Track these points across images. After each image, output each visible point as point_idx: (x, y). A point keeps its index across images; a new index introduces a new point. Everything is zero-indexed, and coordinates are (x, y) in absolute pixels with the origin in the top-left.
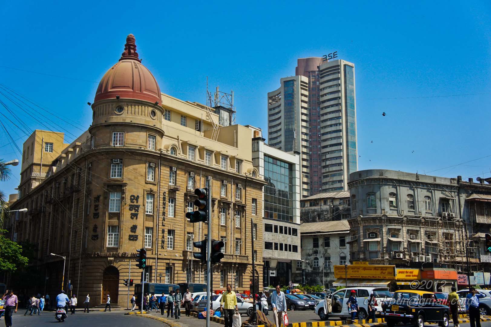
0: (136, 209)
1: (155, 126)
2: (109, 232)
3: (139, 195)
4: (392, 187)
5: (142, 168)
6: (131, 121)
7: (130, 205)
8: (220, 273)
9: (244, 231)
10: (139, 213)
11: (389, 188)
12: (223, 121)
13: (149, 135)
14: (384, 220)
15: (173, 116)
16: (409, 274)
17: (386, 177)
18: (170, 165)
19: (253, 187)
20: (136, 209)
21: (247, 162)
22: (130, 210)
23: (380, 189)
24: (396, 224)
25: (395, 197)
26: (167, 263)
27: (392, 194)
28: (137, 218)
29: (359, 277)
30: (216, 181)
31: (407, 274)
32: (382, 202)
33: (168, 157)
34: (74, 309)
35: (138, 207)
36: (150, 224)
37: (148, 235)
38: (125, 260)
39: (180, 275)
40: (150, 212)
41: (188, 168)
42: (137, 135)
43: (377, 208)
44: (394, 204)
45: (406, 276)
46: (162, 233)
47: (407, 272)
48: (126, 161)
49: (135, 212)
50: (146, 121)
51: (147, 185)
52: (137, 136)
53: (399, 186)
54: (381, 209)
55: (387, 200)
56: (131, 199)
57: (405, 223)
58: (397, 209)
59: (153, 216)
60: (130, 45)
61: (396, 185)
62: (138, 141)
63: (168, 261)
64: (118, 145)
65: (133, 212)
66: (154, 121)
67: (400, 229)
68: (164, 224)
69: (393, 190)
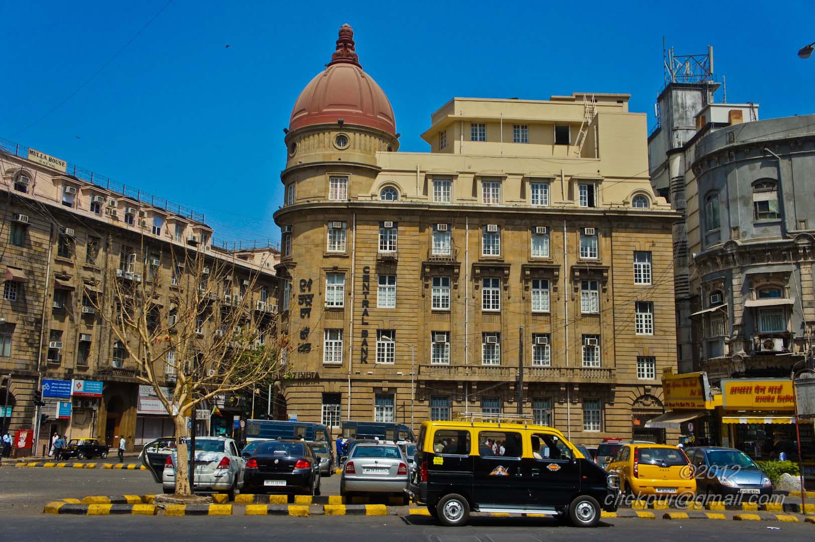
1: (341, 161)
2: (326, 339)
3: (312, 279)
4: (762, 167)
5: (321, 234)
7: (299, 296)
10: (312, 307)
11: (751, 169)
12: (681, 110)
15: (489, 131)
16: (767, 394)
17: (743, 142)
19: (636, 228)
23: (726, 176)
27: (759, 185)
28: (309, 316)
29: (694, 405)
30: (516, 233)
31: (761, 394)
33: (365, 207)
34: (119, 454)
35: (311, 297)
36: (336, 324)
37: (334, 342)
38: (293, 385)
42: (311, 182)
43: (720, 228)
44: (773, 208)
45: (758, 399)
47: (758, 389)
49: (307, 306)
50: (324, 156)
51: (327, 259)
52: (310, 184)
53: (790, 157)
54: (730, 227)
55: (746, 200)
56: (301, 286)
57: (805, 256)
58: (780, 220)
59: (500, 313)
60: (345, 41)
61: (774, 157)
62: (312, 192)
63: (376, 384)
65: (304, 306)
66: (340, 152)
67: (788, 274)
68: (365, 321)
69: (769, 173)
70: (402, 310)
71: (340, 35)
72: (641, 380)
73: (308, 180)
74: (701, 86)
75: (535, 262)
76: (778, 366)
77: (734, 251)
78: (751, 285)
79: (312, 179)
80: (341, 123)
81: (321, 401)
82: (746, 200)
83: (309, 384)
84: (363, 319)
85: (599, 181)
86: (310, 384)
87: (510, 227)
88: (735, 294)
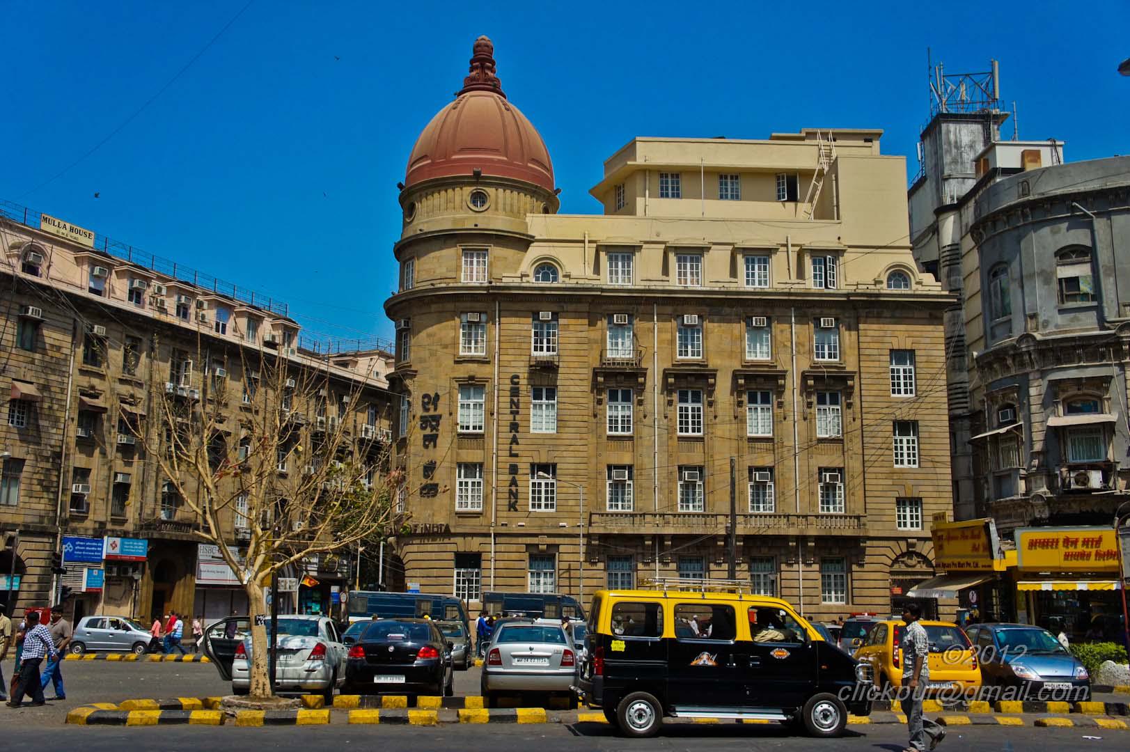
0: (434, 423)
5: (451, 330)
6: (476, 225)
7: (421, 417)
8: (816, 567)
9: (856, 446)
11: (1054, 233)
12: (954, 151)
13: (463, 250)
14: (1029, 353)
15: (684, 184)
16: (1080, 548)
17: (1043, 194)
18: (534, 309)
20: (434, 423)
21: (879, 250)
22: (423, 428)
23: (1019, 243)
24: (1088, 361)
25: (1087, 259)
26: (528, 546)
27: (1066, 254)
28: (435, 446)
29: (977, 566)
30: (724, 326)
31: (1071, 549)
32: (1026, 289)
35: (437, 419)
37: (470, 481)
39: (577, 574)
40: (474, 428)
41: (604, 307)
44: (1085, 287)
45: (1067, 556)
46: (510, 474)
47: (1067, 542)
48: (416, 320)
49: (432, 431)
50: (455, 221)
52: (435, 260)
54: (1025, 315)
55: (1047, 277)
56: (424, 404)
60: (482, 59)
61: (1085, 215)
62: (438, 271)
63: (529, 540)
64: (620, 282)
65: (428, 431)
66: (477, 215)
67: (1108, 379)
68: (513, 452)
69: (1080, 237)
70: (565, 436)
71: (475, 52)
72: (903, 531)
73: (432, 255)
74: (982, 116)
75: (752, 366)
76: (1095, 509)
77: (1032, 348)
78: (1056, 395)
79: (437, 253)
80: (477, 175)
81: (452, 564)
82: (1047, 277)
83: (436, 540)
84: (511, 449)
85: (837, 253)
86: (438, 541)
87: (716, 318)
88: (1033, 408)
